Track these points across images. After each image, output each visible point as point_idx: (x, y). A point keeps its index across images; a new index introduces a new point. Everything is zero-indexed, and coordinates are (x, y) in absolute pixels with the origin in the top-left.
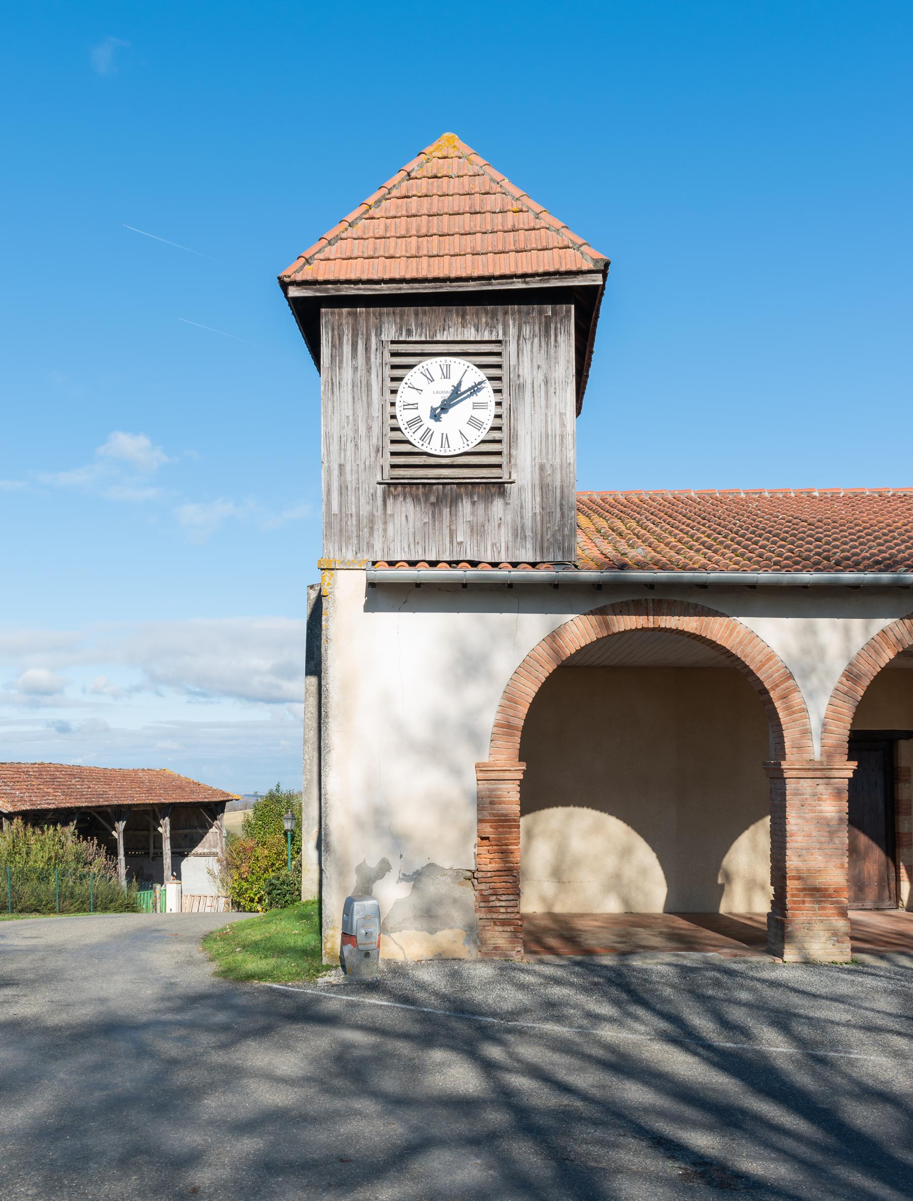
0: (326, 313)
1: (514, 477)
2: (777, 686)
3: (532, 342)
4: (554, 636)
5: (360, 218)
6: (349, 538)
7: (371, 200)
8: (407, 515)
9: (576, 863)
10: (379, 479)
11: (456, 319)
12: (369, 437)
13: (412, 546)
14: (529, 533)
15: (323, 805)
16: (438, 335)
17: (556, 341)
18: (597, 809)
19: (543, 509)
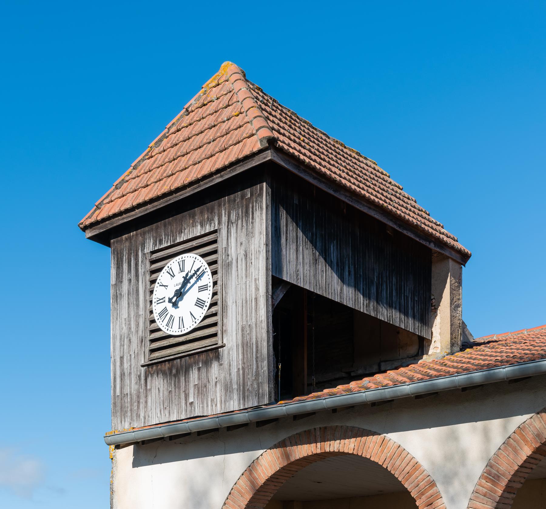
0: (114, 243)
2: (423, 494)
3: (237, 225)
4: (251, 469)
5: (143, 160)
6: (126, 412)
7: (152, 144)
10: (142, 362)
13: (162, 410)
14: (235, 386)
16: (178, 238)
17: (253, 218)
19: (244, 363)
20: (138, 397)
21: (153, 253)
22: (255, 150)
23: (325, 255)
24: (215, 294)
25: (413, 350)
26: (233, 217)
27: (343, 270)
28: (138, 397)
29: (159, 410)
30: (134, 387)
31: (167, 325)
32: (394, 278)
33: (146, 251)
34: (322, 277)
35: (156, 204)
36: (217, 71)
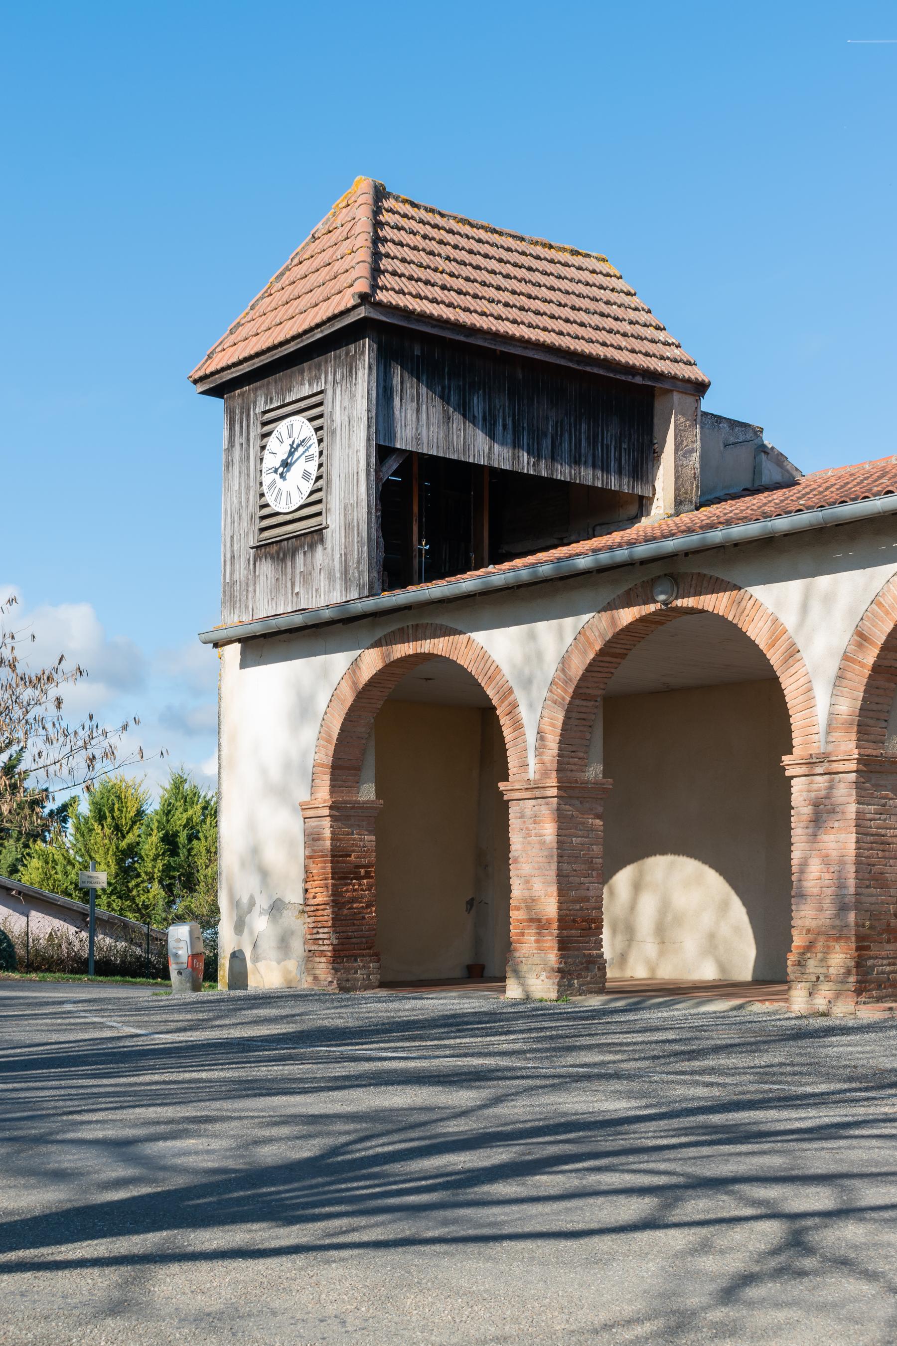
5: (262, 298)
6: (235, 602)
9: (679, 920)
10: (252, 544)
14: (338, 575)
18: (691, 857)
20: (247, 585)
21: (265, 412)
22: (349, 305)
23: (464, 410)
24: (320, 465)
25: (633, 510)
26: (338, 377)
27: (493, 425)
28: (247, 585)
29: (271, 601)
30: (244, 572)
31: (275, 500)
32: (583, 425)
33: (258, 411)
34: (458, 437)
35: (262, 357)
36: (350, 187)
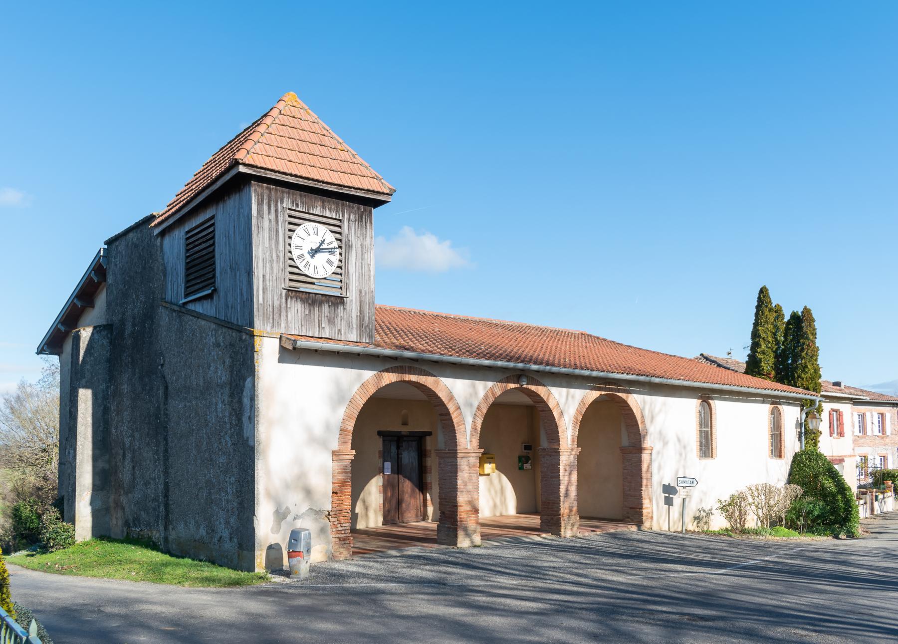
1: (348, 295)
8: (297, 309)
11: (319, 204)
12: (278, 262)
15: (868, 399)
